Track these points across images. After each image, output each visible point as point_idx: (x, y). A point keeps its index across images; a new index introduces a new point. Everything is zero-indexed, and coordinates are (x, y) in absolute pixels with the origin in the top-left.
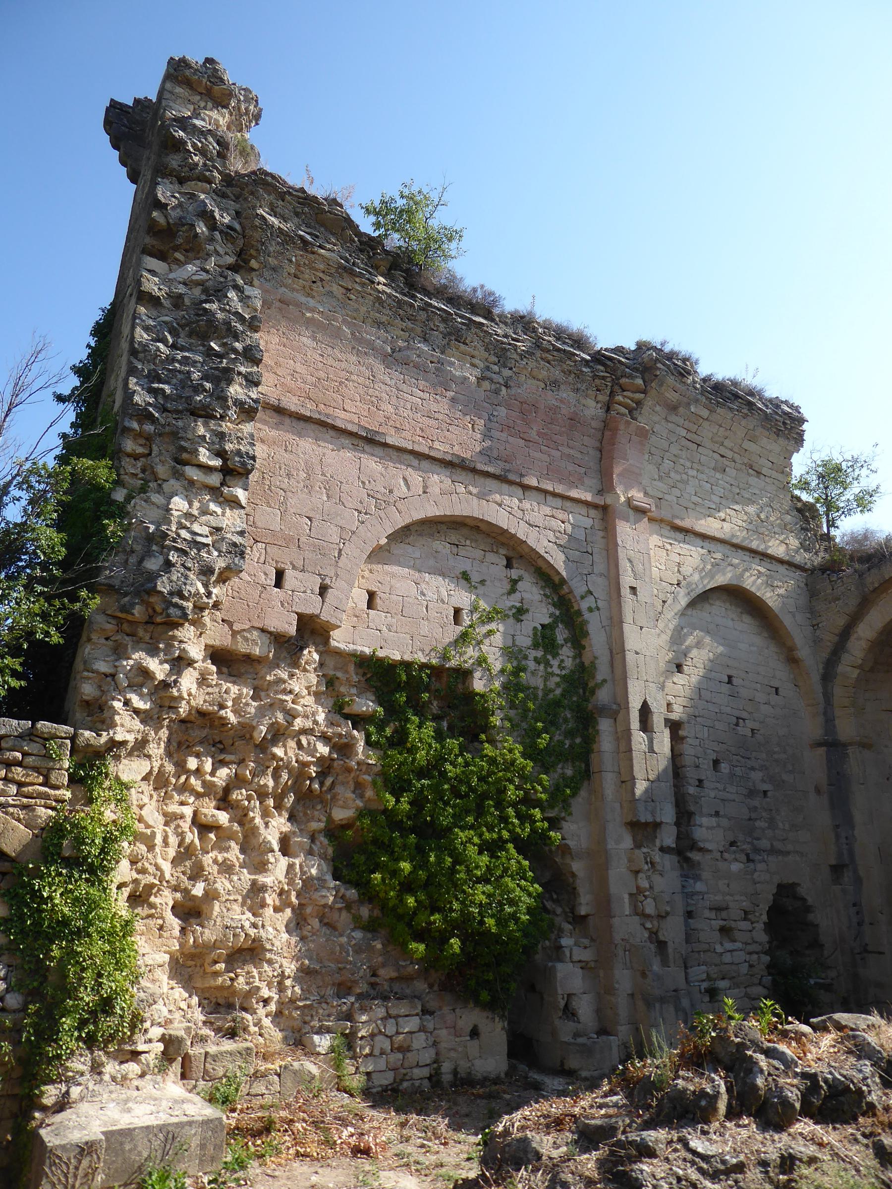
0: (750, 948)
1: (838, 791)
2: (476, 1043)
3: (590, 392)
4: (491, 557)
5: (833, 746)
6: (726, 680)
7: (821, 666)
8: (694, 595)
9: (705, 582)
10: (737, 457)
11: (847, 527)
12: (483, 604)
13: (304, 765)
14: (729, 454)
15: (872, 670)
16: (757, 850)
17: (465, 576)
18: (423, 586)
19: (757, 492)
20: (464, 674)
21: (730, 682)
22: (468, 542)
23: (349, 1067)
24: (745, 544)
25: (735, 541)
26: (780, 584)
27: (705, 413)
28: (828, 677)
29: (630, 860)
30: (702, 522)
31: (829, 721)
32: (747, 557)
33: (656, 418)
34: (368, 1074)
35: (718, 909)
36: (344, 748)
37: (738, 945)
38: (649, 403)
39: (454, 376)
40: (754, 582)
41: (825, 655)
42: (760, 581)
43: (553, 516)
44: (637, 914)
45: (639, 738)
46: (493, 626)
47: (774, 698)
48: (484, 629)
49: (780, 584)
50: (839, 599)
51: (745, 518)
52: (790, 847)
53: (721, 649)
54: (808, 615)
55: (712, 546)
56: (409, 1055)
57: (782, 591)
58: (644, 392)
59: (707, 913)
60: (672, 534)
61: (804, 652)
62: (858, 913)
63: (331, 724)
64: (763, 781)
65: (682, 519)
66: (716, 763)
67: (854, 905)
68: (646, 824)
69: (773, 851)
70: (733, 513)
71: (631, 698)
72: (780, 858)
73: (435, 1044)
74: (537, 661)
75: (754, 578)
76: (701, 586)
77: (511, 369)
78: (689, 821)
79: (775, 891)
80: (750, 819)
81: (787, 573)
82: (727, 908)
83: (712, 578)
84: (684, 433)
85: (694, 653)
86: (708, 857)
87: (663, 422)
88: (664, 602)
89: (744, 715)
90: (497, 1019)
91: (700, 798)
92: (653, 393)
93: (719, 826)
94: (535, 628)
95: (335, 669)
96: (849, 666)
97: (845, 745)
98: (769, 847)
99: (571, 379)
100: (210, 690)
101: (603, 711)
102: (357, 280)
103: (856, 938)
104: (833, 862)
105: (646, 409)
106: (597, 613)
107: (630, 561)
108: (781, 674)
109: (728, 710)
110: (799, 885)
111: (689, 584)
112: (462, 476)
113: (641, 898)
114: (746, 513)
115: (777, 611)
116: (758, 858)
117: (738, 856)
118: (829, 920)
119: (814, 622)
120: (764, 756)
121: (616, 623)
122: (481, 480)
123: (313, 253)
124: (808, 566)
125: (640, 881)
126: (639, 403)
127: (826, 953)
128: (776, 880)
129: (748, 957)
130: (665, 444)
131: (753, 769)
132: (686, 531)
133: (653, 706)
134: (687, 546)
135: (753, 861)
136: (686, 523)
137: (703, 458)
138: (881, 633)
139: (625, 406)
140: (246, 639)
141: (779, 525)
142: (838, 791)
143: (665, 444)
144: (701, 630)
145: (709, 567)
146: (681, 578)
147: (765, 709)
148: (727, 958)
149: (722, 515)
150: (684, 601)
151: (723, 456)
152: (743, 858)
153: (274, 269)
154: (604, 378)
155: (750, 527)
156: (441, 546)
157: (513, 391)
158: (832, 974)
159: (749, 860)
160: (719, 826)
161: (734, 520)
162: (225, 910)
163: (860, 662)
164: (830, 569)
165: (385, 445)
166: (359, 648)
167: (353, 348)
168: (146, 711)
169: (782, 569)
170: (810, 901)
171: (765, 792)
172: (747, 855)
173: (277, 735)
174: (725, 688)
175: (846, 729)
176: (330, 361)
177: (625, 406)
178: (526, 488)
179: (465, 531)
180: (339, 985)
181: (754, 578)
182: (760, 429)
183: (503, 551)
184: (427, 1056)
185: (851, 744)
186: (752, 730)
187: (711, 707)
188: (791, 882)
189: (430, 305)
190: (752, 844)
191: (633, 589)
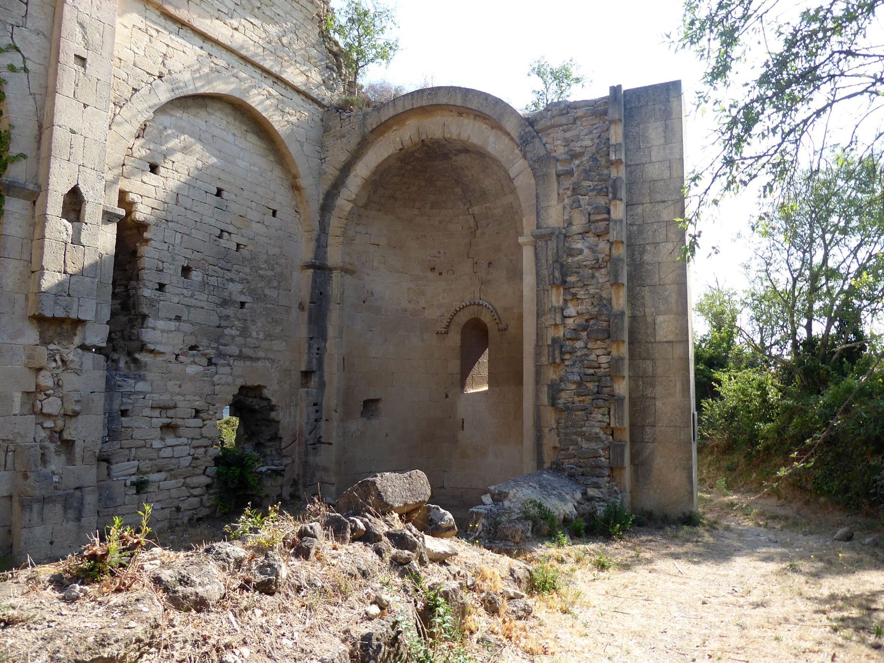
0: (196, 443)
1: (318, 308)
5: (319, 268)
6: (215, 192)
7: (321, 197)
8: (179, 93)
9: (198, 84)
11: (373, 76)
15: (365, 206)
16: (221, 355)
19: (282, 14)
21: (219, 193)
24: (257, 60)
25: (243, 52)
26: (291, 111)
28: (326, 207)
29: (30, 357)
30: (208, 22)
31: (321, 246)
32: (258, 75)
35: (164, 408)
37: (180, 441)
40: (262, 102)
41: (325, 186)
42: (268, 102)
44: (34, 413)
45: (58, 227)
47: (269, 218)
49: (291, 111)
50: (344, 136)
51: (264, 35)
52: (261, 354)
53: (213, 160)
54: (318, 149)
55: (215, 50)
57: (293, 119)
59: (147, 412)
60: (162, 20)
61: (306, 181)
62: (317, 411)
64: (241, 292)
65: (176, 7)
66: (186, 271)
67: (315, 405)
68: (62, 321)
69: (241, 357)
70: (248, 25)
71: (53, 180)
72: (248, 363)
75: (261, 97)
76: (192, 87)
78: (143, 324)
79: (236, 392)
80: (219, 327)
81: (302, 103)
82: (175, 407)
83: (209, 82)
85: (178, 157)
86: (160, 358)
88: (135, 90)
89: (231, 229)
91: (158, 302)
93: (178, 330)
96: (344, 203)
97: (331, 270)
98: (237, 352)
101: (13, 189)
103: (310, 433)
104: (303, 369)
106: (23, 75)
108: (282, 198)
109: (212, 221)
110: (265, 387)
111: (173, 82)
113: (42, 396)
114: (265, 31)
115: (283, 136)
116: (222, 361)
117: (197, 359)
118: (291, 418)
119: (323, 156)
120: (247, 270)
121: (46, 94)
124: (325, 102)
127: (283, 445)
128: (240, 382)
129: (192, 451)
131: (231, 280)
132: (183, 24)
134: (180, 40)
135: (216, 365)
136: (182, 14)
138: (374, 173)
141: (303, 56)
142: (318, 308)
144: (191, 136)
145: (206, 70)
146: (165, 71)
147: (256, 227)
148: (168, 452)
149: (235, 23)
150: (164, 95)
152: (204, 361)
155: (268, 46)
158: (286, 461)
159: (210, 362)
160: (178, 330)
161: (248, 33)
163: (354, 196)
164: (342, 108)
169: (297, 99)
170: (274, 401)
171: (242, 304)
172: (210, 360)
174: (213, 200)
175: (334, 256)
181: (261, 97)
185: (335, 269)
186: (238, 245)
187: (189, 214)
188: (256, 384)
190: (217, 349)
191: (81, 60)
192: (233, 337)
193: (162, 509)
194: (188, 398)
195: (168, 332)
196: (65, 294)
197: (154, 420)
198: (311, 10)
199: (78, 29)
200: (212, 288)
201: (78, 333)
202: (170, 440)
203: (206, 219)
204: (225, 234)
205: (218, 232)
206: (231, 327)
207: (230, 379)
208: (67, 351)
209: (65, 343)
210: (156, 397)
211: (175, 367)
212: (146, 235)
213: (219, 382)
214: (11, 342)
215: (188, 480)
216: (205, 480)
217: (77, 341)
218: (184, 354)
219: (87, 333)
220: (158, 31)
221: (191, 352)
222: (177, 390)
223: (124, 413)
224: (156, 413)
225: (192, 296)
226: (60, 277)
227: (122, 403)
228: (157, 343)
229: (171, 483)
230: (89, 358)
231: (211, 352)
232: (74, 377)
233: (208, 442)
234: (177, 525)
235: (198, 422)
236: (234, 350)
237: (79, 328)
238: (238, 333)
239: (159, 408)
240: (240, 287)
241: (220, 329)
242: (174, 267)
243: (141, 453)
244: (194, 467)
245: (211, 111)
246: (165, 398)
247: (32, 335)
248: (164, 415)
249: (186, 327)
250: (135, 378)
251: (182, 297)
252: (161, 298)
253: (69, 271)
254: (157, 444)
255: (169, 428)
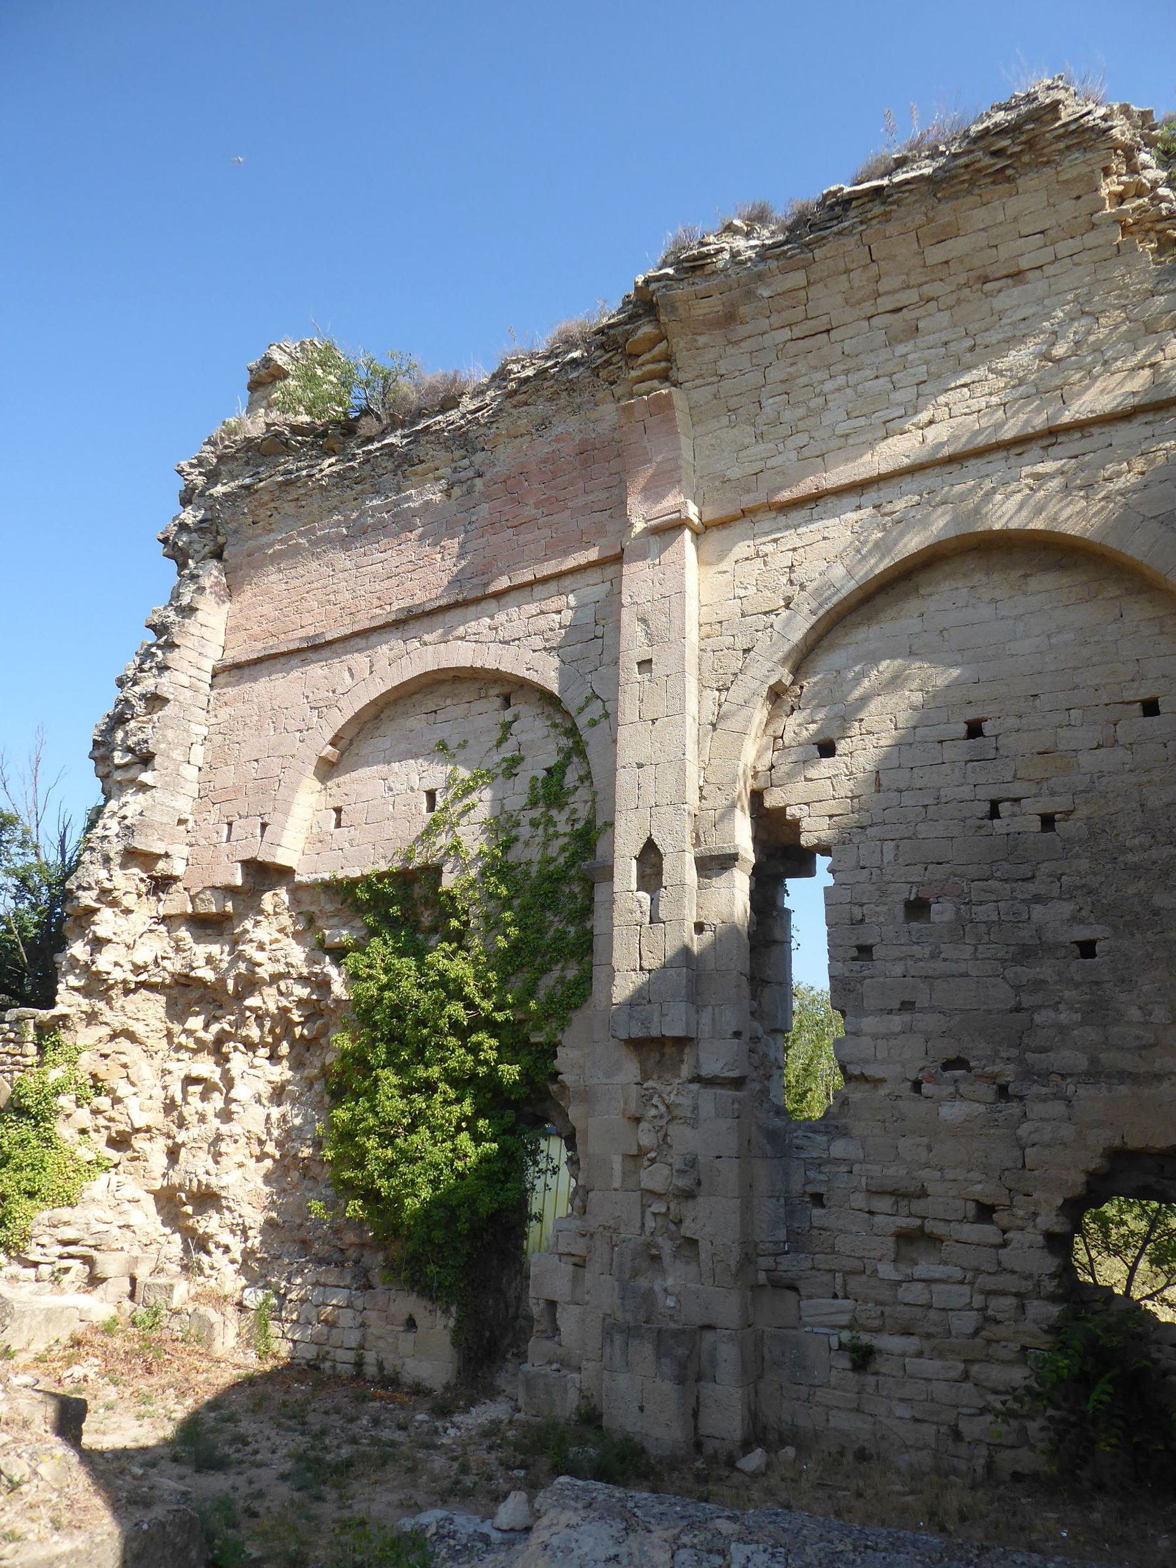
0: (984, 1281)
2: (410, 1336)
3: (600, 395)
4: (479, 706)
10: (927, 290)
12: (464, 773)
13: (284, 1011)
14: (911, 296)
16: (1028, 1074)
17: (443, 746)
18: (391, 779)
20: (434, 872)
22: (449, 702)
23: (274, 1328)
27: (799, 278)
30: (867, 457)
33: (710, 355)
34: (294, 1342)
36: (322, 984)
38: (680, 345)
39: (415, 508)
43: (542, 612)
46: (473, 797)
48: (459, 807)
55: (886, 491)
56: (334, 1331)
58: (663, 337)
63: (311, 961)
64: (1075, 919)
69: (1094, 1074)
72: (1123, 1089)
73: (363, 1325)
74: (534, 824)
77: (483, 449)
80: (1018, 1009)
82: (923, 1194)
84: (786, 334)
87: (730, 350)
89: (1017, 790)
90: (439, 1313)
92: (673, 328)
93: (908, 1030)
94: (535, 779)
95: (312, 903)
99: (564, 399)
100: (185, 954)
102: (299, 484)
105: (682, 357)
107: (643, 620)
109: (966, 792)
112: (414, 628)
116: (1036, 1089)
120: (1084, 864)
122: (439, 619)
123: (257, 491)
125: (640, 1134)
126: (668, 358)
130: (755, 378)
132: (815, 499)
133: (664, 844)
137: (848, 346)
139: (651, 376)
140: (203, 901)
143: (755, 378)
144: (893, 657)
148: (914, 1293)
151: (898, 310)
152: (988, 1092)
153: (236, 532)
154: (608, 363)
156: (416, 722)
157: (488, 476)
159: (1003, 1092)
160: (908, 1030)
162: (190, 1157)
165: (329, 643)
166: (319, 876)
167: (313, 555)
168: (83, 987)
171: (1087, 949)
173: (250, 984)
174: (961, 750)
176: (297, 582)
177: (651, 376)
178: (498, 595)
179: (445, 689)
180: (675, 1257)
182: (944, 207)
183: (494, 691)
184: (353, 1339)
187: (908, 799)
189: (370, 452)
190: (1021, 1061)
192: (1062, 1029)
193: (916, 1420)
194: (950, 1174)
195: (886, 1037)
196: (645, 1002)
197: (878, 1219)
198: (1101, 241)
199: (639, 628)
200: (983, 928)
201: (686, 1057)
202: (925, 1268)
203: (947, 793)
204: (1004, 808)
205: (987, 807)
206: (1055, 1007)
207: (1067, 1132)
208: (669, 1088)
209: (668, 1076)
210: (875, 1170)
211: (912, 1108)
212: (96, 918)
213: (1035, 1138)
214: (608, 1081)
215: (975, 1369)
216: (1018, 1376)
217: (685, 1071)
218: (932, 1079)
219: (702, 1055)
220: (775, 541)
221: (948, 1074)
222: (923, 1155)
223: (818, 1199)
224: (883, 1204)
225: (934, 956)
226: (642, 978)
227: (808, 1182)
228: (866, 1062)
229: (931, 1366)
230: (708, 1099)
231: (1008, 1073)
232: (687, 1131)
233: (1026, 1286)
234: (955, 1471)
235: (988, 1233)
236: (1074, 1059)
237: (687, 1050)
238: (1078, 1017)
239: (892, 1193)
240: (1066, 909)
241: (1023, 1016)
242: (884, 909)
243: (855, 1284)
244: (989, 1342)
245: (929, 590)
246: (895, 1173)
247: (630, 1070)
248: (904, 1211)
249: (929, 1022)
250: (827, 1133)
251: (910, 962)
252: (866, 973)
253: (646, 965)
254: (887, 1271)
255: (911, 1240)
